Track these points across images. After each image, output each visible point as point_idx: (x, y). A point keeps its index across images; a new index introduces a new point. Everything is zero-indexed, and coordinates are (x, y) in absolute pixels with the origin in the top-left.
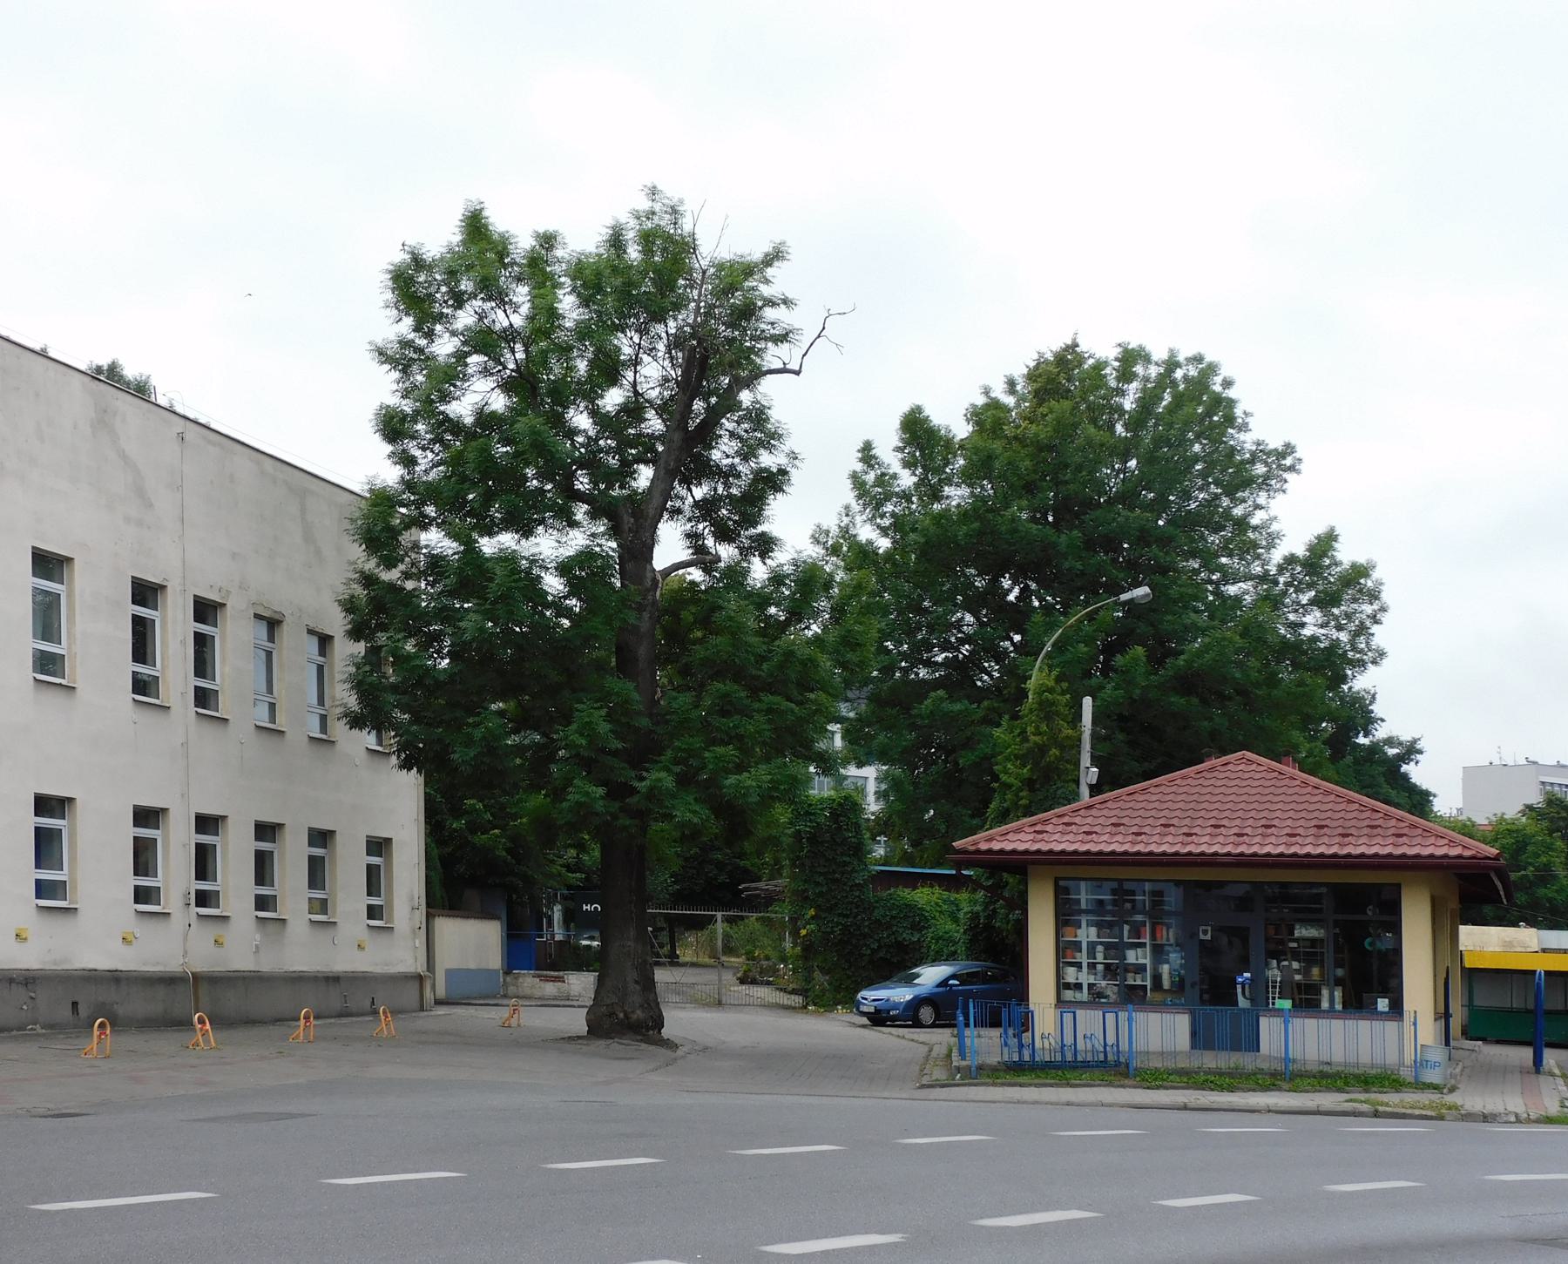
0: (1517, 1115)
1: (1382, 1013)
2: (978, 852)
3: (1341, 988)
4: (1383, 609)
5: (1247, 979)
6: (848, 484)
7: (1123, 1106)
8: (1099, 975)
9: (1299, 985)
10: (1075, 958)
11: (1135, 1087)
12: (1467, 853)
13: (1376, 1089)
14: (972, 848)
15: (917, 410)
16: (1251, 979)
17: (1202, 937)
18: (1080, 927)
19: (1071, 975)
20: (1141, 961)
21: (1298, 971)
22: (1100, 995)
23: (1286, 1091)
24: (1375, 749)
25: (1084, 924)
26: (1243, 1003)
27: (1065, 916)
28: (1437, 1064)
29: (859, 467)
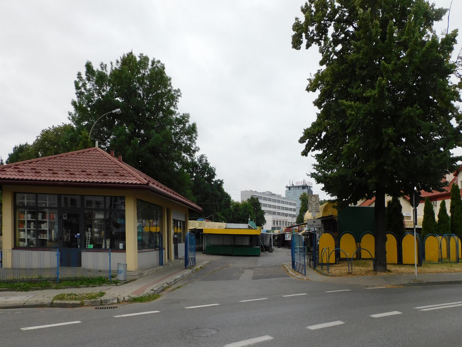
0: (118, 299)
1: (121, 249)
3: (109, 239)
5: (78, 236)
8: (31, 235)
10: (30, 228)
12: (139, 183)
13: (91, 285)
16: (80, 236)
17: (64, 218)
19: (23, 235)
20: (46, 229)
23: (54, 289)
24: (216, 182)
25: (26, 213)
28: (122, 272)
29: (77, 80)
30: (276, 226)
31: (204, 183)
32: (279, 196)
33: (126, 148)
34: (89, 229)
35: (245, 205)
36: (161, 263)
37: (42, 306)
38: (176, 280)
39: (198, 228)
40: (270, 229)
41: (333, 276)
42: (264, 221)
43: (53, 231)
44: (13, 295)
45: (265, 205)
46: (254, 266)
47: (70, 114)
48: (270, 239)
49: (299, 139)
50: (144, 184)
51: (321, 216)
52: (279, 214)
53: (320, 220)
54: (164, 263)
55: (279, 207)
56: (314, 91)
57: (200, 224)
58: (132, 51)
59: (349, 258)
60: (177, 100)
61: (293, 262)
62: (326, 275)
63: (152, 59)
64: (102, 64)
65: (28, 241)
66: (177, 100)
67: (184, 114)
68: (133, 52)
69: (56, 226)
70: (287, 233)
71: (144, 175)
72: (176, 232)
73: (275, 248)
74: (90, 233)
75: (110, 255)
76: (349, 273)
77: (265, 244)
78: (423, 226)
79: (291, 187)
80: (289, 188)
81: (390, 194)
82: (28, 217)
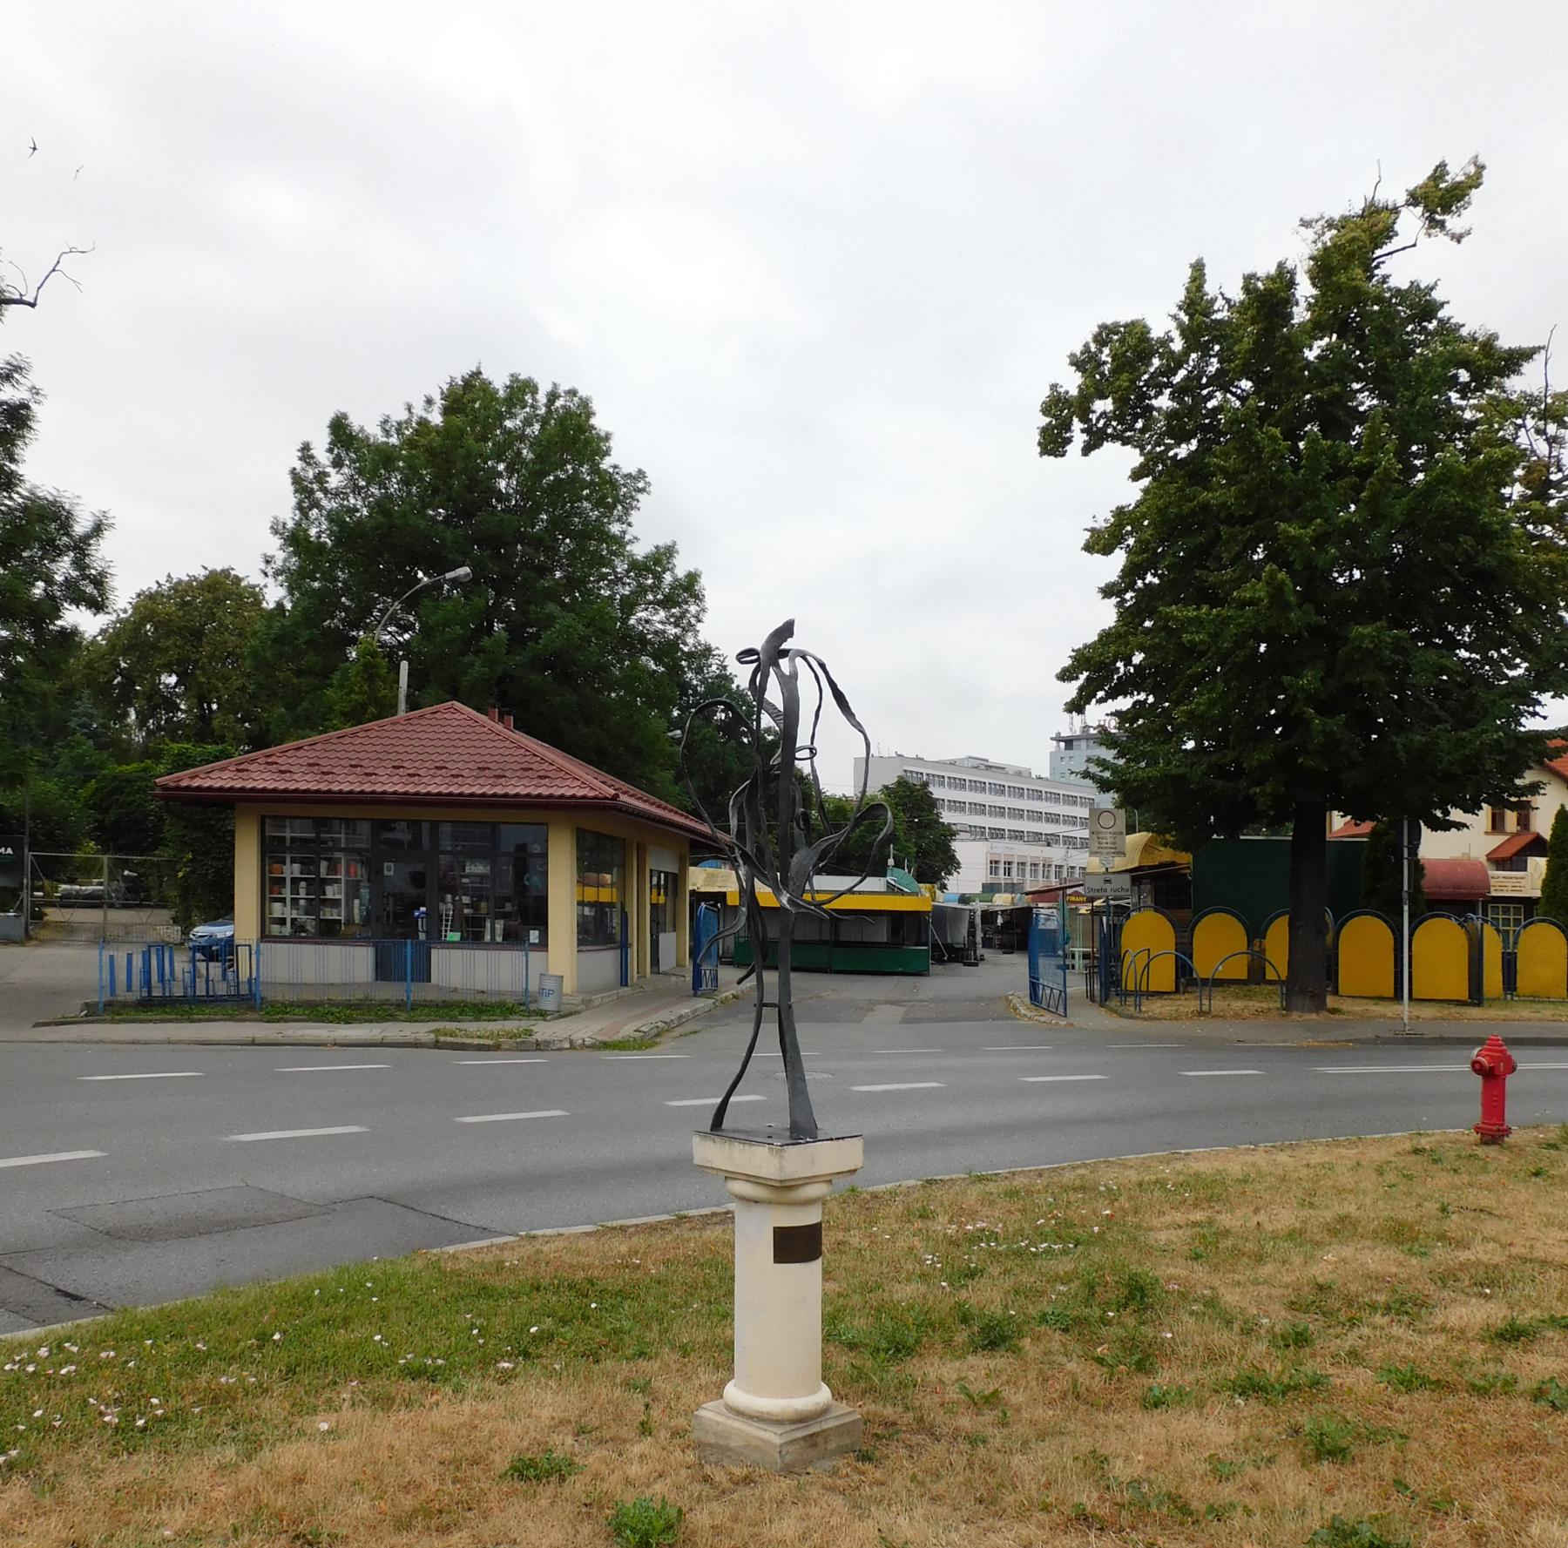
0: (571, 1042)
2: (178, 788)
4: (704, 610)
6: (288, 480)
7: (189, 1043)
9: (467, 918)
11: (256, 1021)
12: (592, 794)
14: (172, 784)
15: (345, 416)
18: (284, 863)
19: (277, 910)
20: (337, 897)
21: (467, 906)
22: (302, 928)
25: (288, 861)
26: (422, 936)
27: (271, 852)
29: (299, 465)
30: (1002, 878)
31: (713, 740)
32: (1019, 773)
33: (466, 660)
34: (449, 897)
35: (869, 812)
36: (624, 981)
37: (417, 1045)
38: (681, 1017)
39: (702, 890)
40: (979, 890)
41: (1151, 1019)
42: (951, 863)
43: (357, 902)
44: (318, 1028)
45: (958, 806)
46: (905, 998)
47: (268, 562)
48: (972, 924)
49: (1059, 670)
50: (607, 798)
51: (1136, 865)
52: (1017, 835)
53: (1127, 877)
54: (629, 982)
55: (1018, 814)
56: (1107, 550)
57: (710, 877)
58: (478, 368)
59: (1202, 980)
60: (635, 503)
61: (1034, 987)
62: (1132, 1017)
63: (549, 388)
64: (386, 422)
65: (292, 924)
66: (635, 503)
67: (657, 547)
68: (482, 370)
69: (365, 892)
70: (1040, 905)
71: (609, 778)
72: (654, 901)
73: (988, 954)
74: (450, 906)
75: (527, 955)
76: (1201, 1013)
77: (949, 941)
78: (1543, 892)
79: (1078, 738)
80: (1069, 742)
81: (1321, 825)
82: (292, 870)
